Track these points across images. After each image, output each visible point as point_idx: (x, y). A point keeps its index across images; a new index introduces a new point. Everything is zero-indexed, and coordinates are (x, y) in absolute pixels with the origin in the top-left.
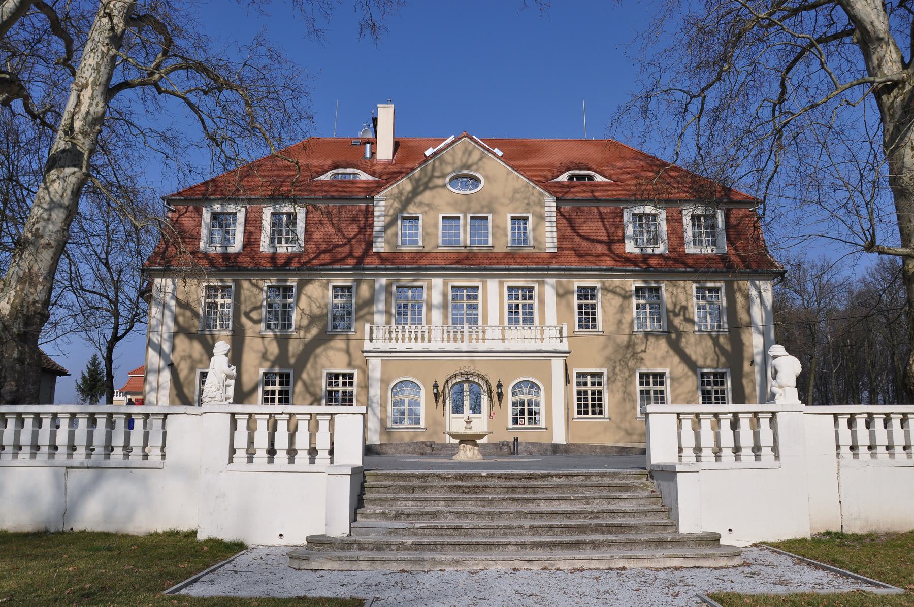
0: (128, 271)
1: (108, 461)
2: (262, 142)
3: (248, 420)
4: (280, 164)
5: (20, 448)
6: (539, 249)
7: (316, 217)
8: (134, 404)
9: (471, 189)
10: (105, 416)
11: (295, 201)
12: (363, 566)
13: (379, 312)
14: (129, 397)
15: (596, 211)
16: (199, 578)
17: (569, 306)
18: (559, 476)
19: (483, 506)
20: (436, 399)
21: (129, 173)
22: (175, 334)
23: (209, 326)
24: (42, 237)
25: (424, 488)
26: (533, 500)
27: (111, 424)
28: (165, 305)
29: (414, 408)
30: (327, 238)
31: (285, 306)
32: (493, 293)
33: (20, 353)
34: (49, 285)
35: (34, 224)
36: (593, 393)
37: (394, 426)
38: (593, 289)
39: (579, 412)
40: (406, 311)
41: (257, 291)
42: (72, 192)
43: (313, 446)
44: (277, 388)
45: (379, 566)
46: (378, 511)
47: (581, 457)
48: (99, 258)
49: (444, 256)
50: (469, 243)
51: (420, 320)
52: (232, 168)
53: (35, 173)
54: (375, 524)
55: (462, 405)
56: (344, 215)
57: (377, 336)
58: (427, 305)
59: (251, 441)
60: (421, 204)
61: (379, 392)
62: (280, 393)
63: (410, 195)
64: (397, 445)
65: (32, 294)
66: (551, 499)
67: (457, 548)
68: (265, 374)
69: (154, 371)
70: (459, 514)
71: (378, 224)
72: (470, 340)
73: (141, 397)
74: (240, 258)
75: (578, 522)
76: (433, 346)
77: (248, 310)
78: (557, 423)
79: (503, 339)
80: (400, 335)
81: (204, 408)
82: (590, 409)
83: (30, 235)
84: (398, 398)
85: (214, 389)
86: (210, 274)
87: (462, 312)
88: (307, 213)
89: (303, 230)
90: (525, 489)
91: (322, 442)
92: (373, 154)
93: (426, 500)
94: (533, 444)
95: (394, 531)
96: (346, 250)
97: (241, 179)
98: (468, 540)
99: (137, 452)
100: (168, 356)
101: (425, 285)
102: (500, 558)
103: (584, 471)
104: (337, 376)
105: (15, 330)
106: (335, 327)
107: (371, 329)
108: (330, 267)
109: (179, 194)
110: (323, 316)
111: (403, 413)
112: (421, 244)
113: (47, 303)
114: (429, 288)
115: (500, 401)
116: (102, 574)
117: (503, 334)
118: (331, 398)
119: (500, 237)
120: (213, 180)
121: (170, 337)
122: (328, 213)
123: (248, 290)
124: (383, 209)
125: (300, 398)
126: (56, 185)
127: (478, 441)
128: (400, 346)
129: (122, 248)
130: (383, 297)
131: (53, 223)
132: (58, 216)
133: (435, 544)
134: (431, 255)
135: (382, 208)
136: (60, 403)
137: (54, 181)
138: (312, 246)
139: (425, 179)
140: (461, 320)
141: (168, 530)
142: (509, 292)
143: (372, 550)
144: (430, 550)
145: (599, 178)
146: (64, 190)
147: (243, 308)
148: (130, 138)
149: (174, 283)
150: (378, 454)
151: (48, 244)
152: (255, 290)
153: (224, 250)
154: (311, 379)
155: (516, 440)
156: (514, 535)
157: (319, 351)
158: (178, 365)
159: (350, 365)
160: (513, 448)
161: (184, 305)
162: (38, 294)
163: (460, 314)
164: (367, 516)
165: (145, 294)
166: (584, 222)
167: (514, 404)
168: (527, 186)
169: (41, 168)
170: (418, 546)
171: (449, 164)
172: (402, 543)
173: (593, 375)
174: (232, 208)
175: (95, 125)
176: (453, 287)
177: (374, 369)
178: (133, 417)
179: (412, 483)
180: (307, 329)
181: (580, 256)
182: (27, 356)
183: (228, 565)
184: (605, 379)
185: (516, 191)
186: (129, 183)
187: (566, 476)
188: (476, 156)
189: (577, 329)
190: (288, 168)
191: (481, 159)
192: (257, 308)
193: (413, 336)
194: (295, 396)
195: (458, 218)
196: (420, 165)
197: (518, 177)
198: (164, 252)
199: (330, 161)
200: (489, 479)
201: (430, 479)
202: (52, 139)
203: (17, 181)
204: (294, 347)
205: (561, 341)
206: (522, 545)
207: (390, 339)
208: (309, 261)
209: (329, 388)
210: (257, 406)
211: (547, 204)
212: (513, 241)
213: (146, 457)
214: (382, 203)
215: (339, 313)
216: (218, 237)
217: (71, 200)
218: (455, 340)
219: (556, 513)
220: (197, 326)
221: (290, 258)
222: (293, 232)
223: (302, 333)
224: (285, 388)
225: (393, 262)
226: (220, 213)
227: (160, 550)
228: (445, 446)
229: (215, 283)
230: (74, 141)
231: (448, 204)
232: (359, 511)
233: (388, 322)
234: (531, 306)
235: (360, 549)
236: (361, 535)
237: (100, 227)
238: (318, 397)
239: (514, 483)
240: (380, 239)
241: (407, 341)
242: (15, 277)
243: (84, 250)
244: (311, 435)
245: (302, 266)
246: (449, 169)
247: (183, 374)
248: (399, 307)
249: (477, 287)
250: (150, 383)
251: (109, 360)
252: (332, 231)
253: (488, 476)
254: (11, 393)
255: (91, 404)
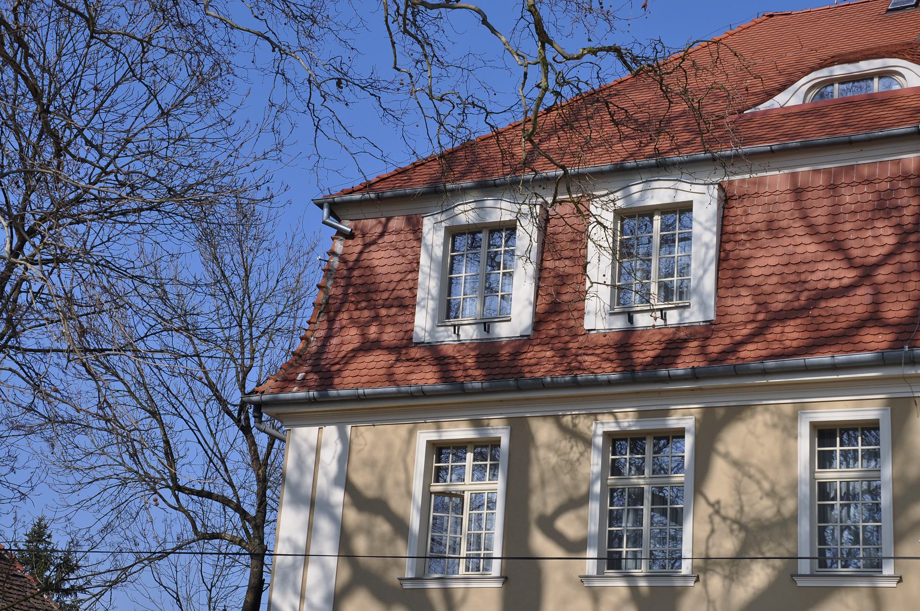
41: (572, 451)
56: (848, 197)
74: (531, 355)
96: (858, 303)
109: (368, 186)
123: (549, 447)
138: (742, 305)
149: (342, 436)
153: (485, 335)
174: (501, 210)
180: (736, 563)
192: (576, 503)
208: (737, 346)
221: (673, 345)
223: (716, 583)
229: (458, 431)
252: (810, 248)
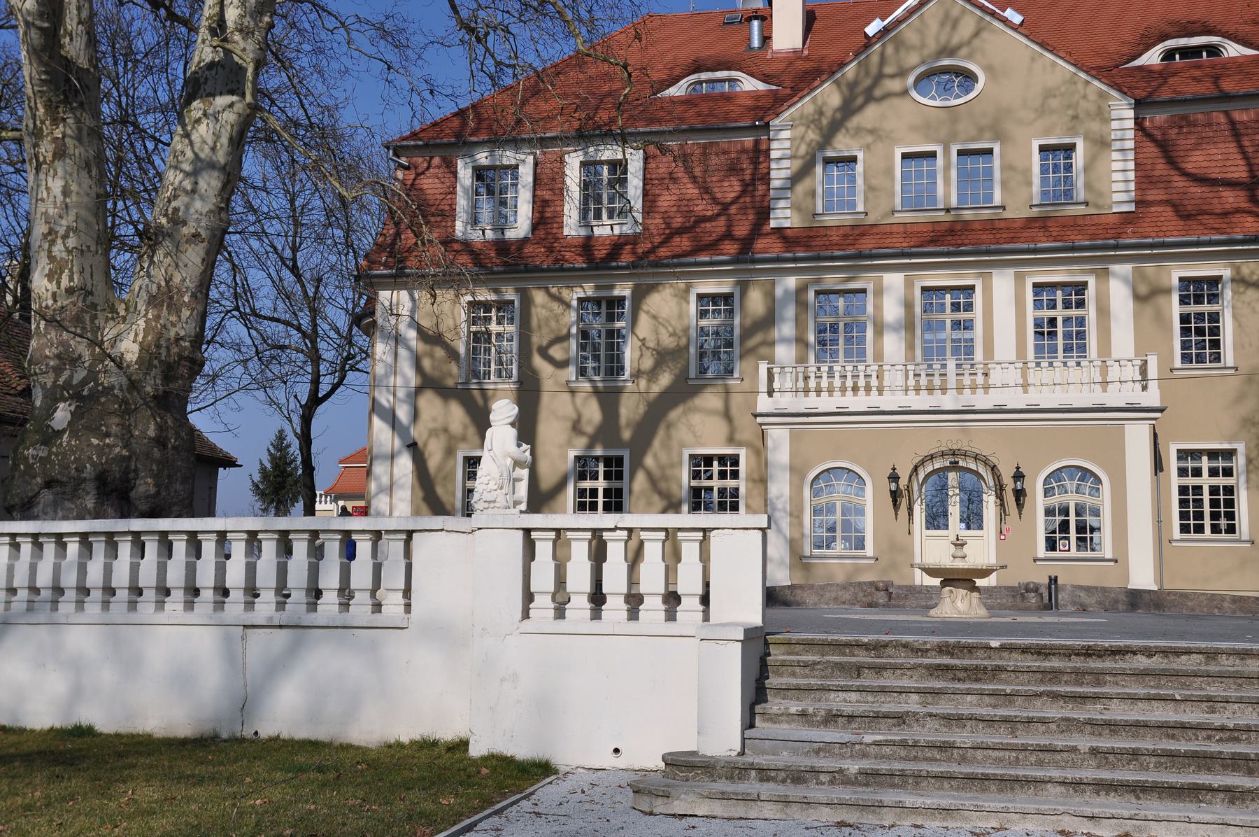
0: (331, 280)
1: (313, 615)
2: (558, 28)
3: (555, 542)
4: (592, 71)
5: (167, 592)
6: (1097, 206)
7: (663, 166)
8: (351, 515)
9: (958, 97)
10: (306, 536)
11: (623, 139)
12: (768, 810)
13: (784, 340)
14: (341, 503)
15: (1223, 119)
16: (475, 824)
17: (1161, 319)
18: (1149, 653)
19: (995, 706)
20: (895, 502)
21: (326, 100)
22: (419, 390)
23: (476, 374)
24: (185, 223)
25: (879, 669)
26: (1096, 698)
27: (317, 552)
28: (398, 339)
29: (852, 518)
30: (683, 204)
31: (610, 333)
32: (1004, 299)
33: (160, 428)
34: (200, 308)
35: (169, 201)
36: (1214, 490)
37: (816, 552)
38: (1215, 281)
39: (1185, 529)
40: (833, 337)
41: (559, 309)
42: (231, 139)
43: (671, 588)
44: (601, 484)
45: (795, 811)
46: (793, 710)
47: (1189, 617)
48: (282, 259)
49: (907, 230)
50: (954, 202)
51: (862, 353)
52: (509, 81)
53: (163, 109)
54: (786, 733)
55: (945, 514)
56: (714, 160)
57: (781, 383)
58: (875, 325)
59: (560, 581)
60: (859, 130)
61: (786, 490)
62: (607, 492)
63: (838, 115)
64: (823, 588)
65: (173, 325)
66: (1134, 699)
67: (946, 785)
68: (578, 458)
69: (383, 457)
70: (948, 719)
71: (779, 174)
72: (960, 389)
73: (362, 503)
74: (528, 249)
75: (1193, 746)
76: (889, 401)
77: (545, 343)
78: (1138, 547)
79: (1025, 386)
80: (825, 383)
81: (477, 520)
82: (1207, 522)
83: (164, 221)
84: (823, 500)
85: (492, 486)
86: (477, 281)
87: (942, 336)
88: (646, 159)
89: (640, 192)
90: (1079, 674)
91: (689, 583)
92: (766, 39)
93: (883, 690)
94: (1088, 589)
95: (824, 748)
96: (719, 226)
97: (525, 101)
98: (965, 769)
99: (362, 599)
100: (408, 429)
101: (870, 287)
102: (1031, 807)
103: (1203, 645)
104: (708, 460)
105: (149, 389)
106: (703, 370)
107: (770, 372)
108: (691, 259)
109: (414, 135)
110: (680, 351)
111: (832, 529)
112: (860, 208)
113: (199, 340)
114: (879, 292)
115: (1020, 506)
116: (311, 812)
117: (1024, 376)
118: (698, 500)
119: (1016, 189)
120: (474, 106)
121: (408, 395)
122: (685, 158)
123: (543, 307)
124: (787, 144)
125: (642, 503)
126: (202, 128)
127: (980, 582)
128: (825, 403)
129: (320, 239)
130: (790, 311)
131: (202, 198)
132: (210, 183)
133: (903, 774)
134: (881, 229)
135: (785, 143)
136: (226, 515)
137: (198, 121)
138: (656, 222)
139: (867, 82)
140: (942, 351)
141: (418, 738)
142: (1036, 294)
143: (784, 781)
144: (893, 786)
145: (1233, 50)
146: (217, 136)
147: (536, 340)
148: (323, 36)
150: (786, 604)
151: (196, 236)
152: (555, 306)
153: (500, 236)
154: (662, 468)
155: (1053, 580)
156: (1057, 765)
157: (674, 415)
158: (425, 445)
159: (731, 440)
160: (1048, 596)
161: (432, 338)
162: (182, 325)
163: (939, 341)
164: (774, 719)
165: (364, 319)
166: (1196, 146)
167: (1049, 512)
168: (1072, 80)
169: (172, 100)
170: (870, 778)
171: (913, 48)
172: (841, 771)
173: (1213, 455)
174: (509, 157)
175: (262, 14)
176: (924, 289)
177: (775, 448)
178: (354, 537)
179: (858, 659)
180: (652, 374)
181: (1185, 215)
182: (171, 433)
183: (524, 803)
184: (1240, 462)
185: (1049, 94)
186: (326, 121)
187: (1165, 652)
188: (967, 27)
189: (1178, 363)
190: (608, 77)
191: (977, 34)
192: (562, 339)
193: (849, 383)
194: (633, 499)
195: (933, 155)
196: (857, 55)
197: (1054, 64)
198: (393, 243)
199: (685, 58)
200: (1005, 654)
201: (890, 651)
202: (188, 45)
203: (135, 125)
204: (630, 409)
205: (1145, 388)
206: (1077, 785)
207: (806, 391)
208: (653, 250)
209: (694, 483)
210: (565, 516)
211: (1114, 114)
212: (1044, 193)
213: (377, 607)
214: (786, 134)
215: (710, 344)
216: (486, 212)
217: (229, 154)
218: (930, 389)
219: (1146, 725)
220: (455, 374)
221: (618, 245)
222: (621, 195)
223: (643, 383)
224: (615, 484)
225: (808, 245)
226: (488, 168)
227: (406, 773)
228: (913, 590)
229: (485, 295)
230: (229, 46)
231: (914, 128)
232: (758, 709)
233: (802, 360)
234: (1081, 321)
235: (761, 780)
236: (763, 753)
237: (279, 202)
238: (674, 500)
239: (1055, 663)
240: (782, 204)
241: (837, 394)
242: (144, 295)
243: (255, 244)
244: (667, 567)
245: (641, 258)
246: (912, 59)
247: (434, 460)
248: (821, 330)
249: (972, 288)
250: (378, 479)
251: (306, 439)
252: (692, 191)
253: (1003, 648)
254: (148, 497)
255: (277, 515)
